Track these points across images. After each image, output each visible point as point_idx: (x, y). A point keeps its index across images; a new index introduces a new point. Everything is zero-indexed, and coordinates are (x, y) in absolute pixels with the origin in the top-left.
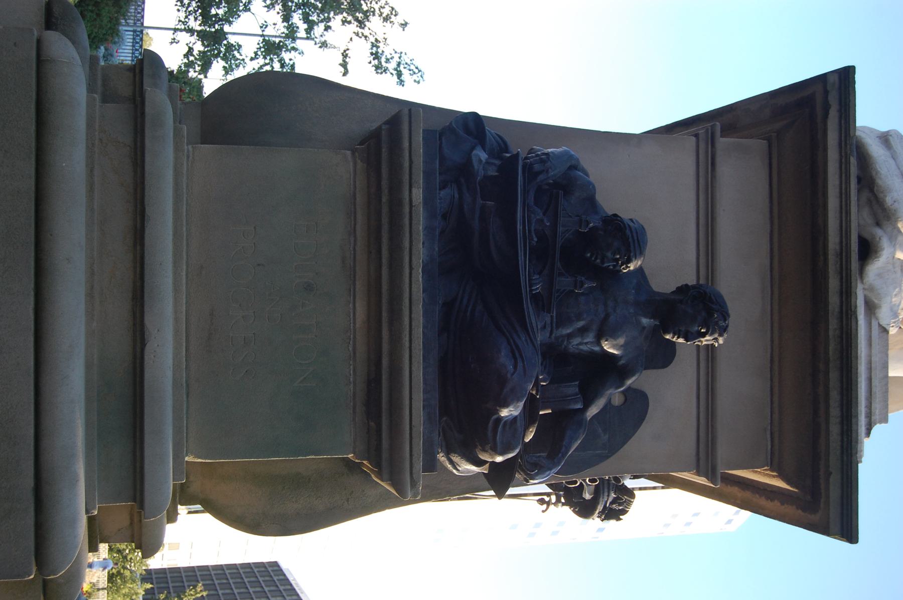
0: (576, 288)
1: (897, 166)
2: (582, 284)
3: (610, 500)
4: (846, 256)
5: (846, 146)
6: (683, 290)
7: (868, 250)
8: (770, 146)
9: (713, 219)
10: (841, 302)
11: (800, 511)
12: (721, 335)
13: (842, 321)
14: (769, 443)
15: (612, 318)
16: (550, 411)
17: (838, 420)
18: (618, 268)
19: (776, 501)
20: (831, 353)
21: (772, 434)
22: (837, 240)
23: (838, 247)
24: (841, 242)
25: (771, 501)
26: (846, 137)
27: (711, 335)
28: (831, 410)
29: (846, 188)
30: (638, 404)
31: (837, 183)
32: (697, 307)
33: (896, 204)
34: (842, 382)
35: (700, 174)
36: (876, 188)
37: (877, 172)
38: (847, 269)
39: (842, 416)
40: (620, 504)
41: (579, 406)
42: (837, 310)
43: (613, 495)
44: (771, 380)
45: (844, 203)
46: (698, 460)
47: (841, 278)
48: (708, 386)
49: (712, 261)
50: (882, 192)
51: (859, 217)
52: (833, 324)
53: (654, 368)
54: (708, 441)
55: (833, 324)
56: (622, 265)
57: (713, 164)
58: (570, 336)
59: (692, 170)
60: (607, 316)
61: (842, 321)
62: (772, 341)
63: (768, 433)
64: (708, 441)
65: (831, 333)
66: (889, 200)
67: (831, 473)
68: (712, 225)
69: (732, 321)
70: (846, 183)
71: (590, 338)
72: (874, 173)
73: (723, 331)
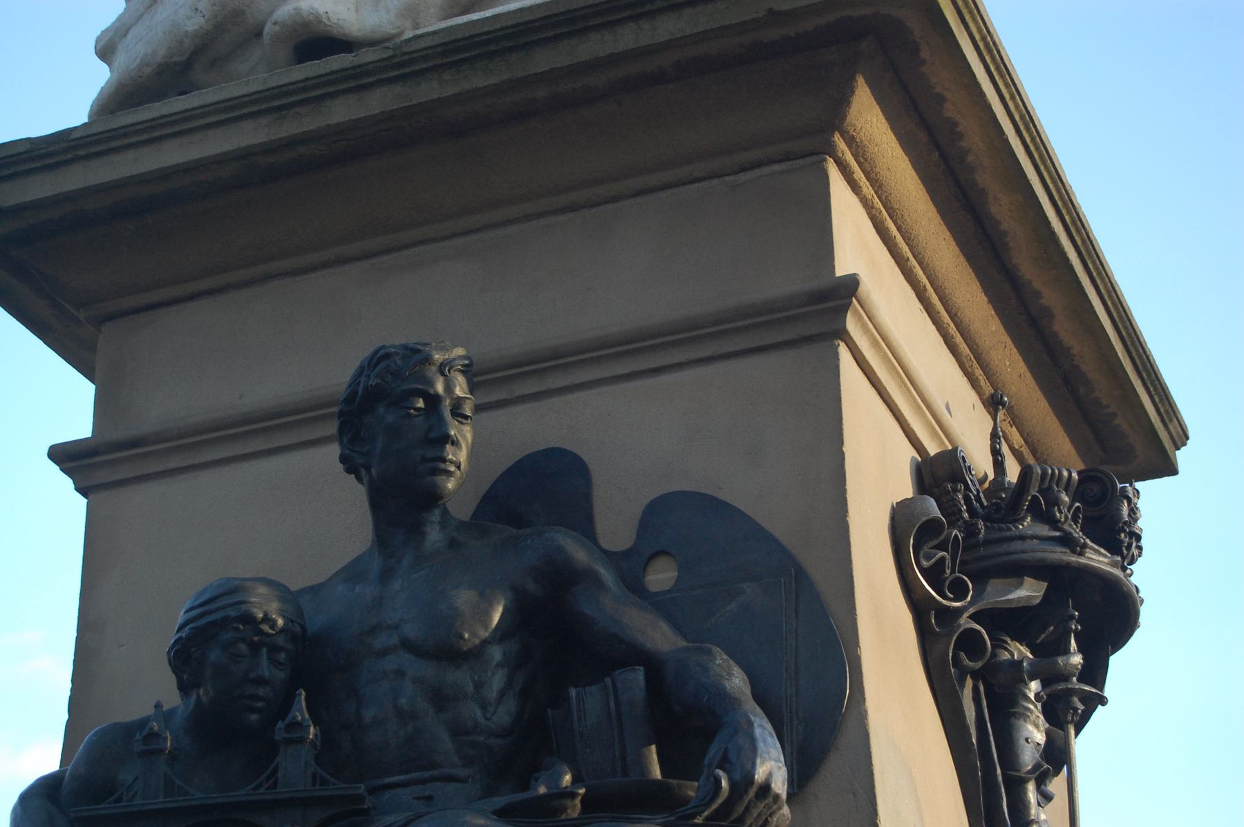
0: (302, 740)
1: (134, 24)
2: (296, 725)
3: (1045, 531)
4: (273, 98)
5: (51, 155)
6: (350, 465)
7: (316, 42)
8: (110, 318)
9: (248, 419)
10: (381, 83)
11: (925, 54)
12: (428, 360)
13: (422, 72)
14: (766, 170)
15: (411, 631)
16: (653, 747)
17: (645, 25)
18: (280, 640)
19: (948, 114)
20: (493, 80)
21: (743, 169)
22: (248, 125)
23: (264, 121)
24: (252, 115)
25: (955, 124)
26: (32, 159)
27: (431, 383)
28: (621, 47)
29: (138, 132)
30: (685, 519)
31: (130, 155)
32: (382, 423)
33: (201, 6)
34: (557, 38)
35: (160, 468)
36: (176, 59)
37: (144, 64)
38: (304, 90)
39: (636, 18)
40: (1054, 502)
41: (637, 677)
42: (398, 89)
43: (1027, 525)
44: (615, 199)
45: (202, 122)
46: (809, 339)
47: (332, 96)
48: (673, 344)
49: (653, 336)
50: (181, 43)
51: (253, 75)
52: (429, 91)
53: (587, 497)
54: (754, 326)
55: (429, 91)
56: (261, 633)
57: (134, 443)
58: (458, 731)
59: (156, 490)
60: (408, 645)
61: (422, 72)
62: (528, 218)
63: (743, 177)
64: (754, 326)
65: (449, 91)
66: (194, 24)
67: (770, 10)
68: (312, 408)
69: (396, 337)
70: (125, 135)
71: (460, 677)
72: (148, 70)
73: (416, 356)
